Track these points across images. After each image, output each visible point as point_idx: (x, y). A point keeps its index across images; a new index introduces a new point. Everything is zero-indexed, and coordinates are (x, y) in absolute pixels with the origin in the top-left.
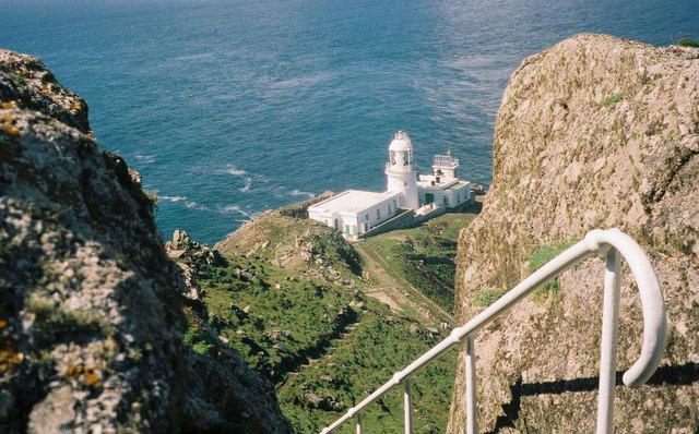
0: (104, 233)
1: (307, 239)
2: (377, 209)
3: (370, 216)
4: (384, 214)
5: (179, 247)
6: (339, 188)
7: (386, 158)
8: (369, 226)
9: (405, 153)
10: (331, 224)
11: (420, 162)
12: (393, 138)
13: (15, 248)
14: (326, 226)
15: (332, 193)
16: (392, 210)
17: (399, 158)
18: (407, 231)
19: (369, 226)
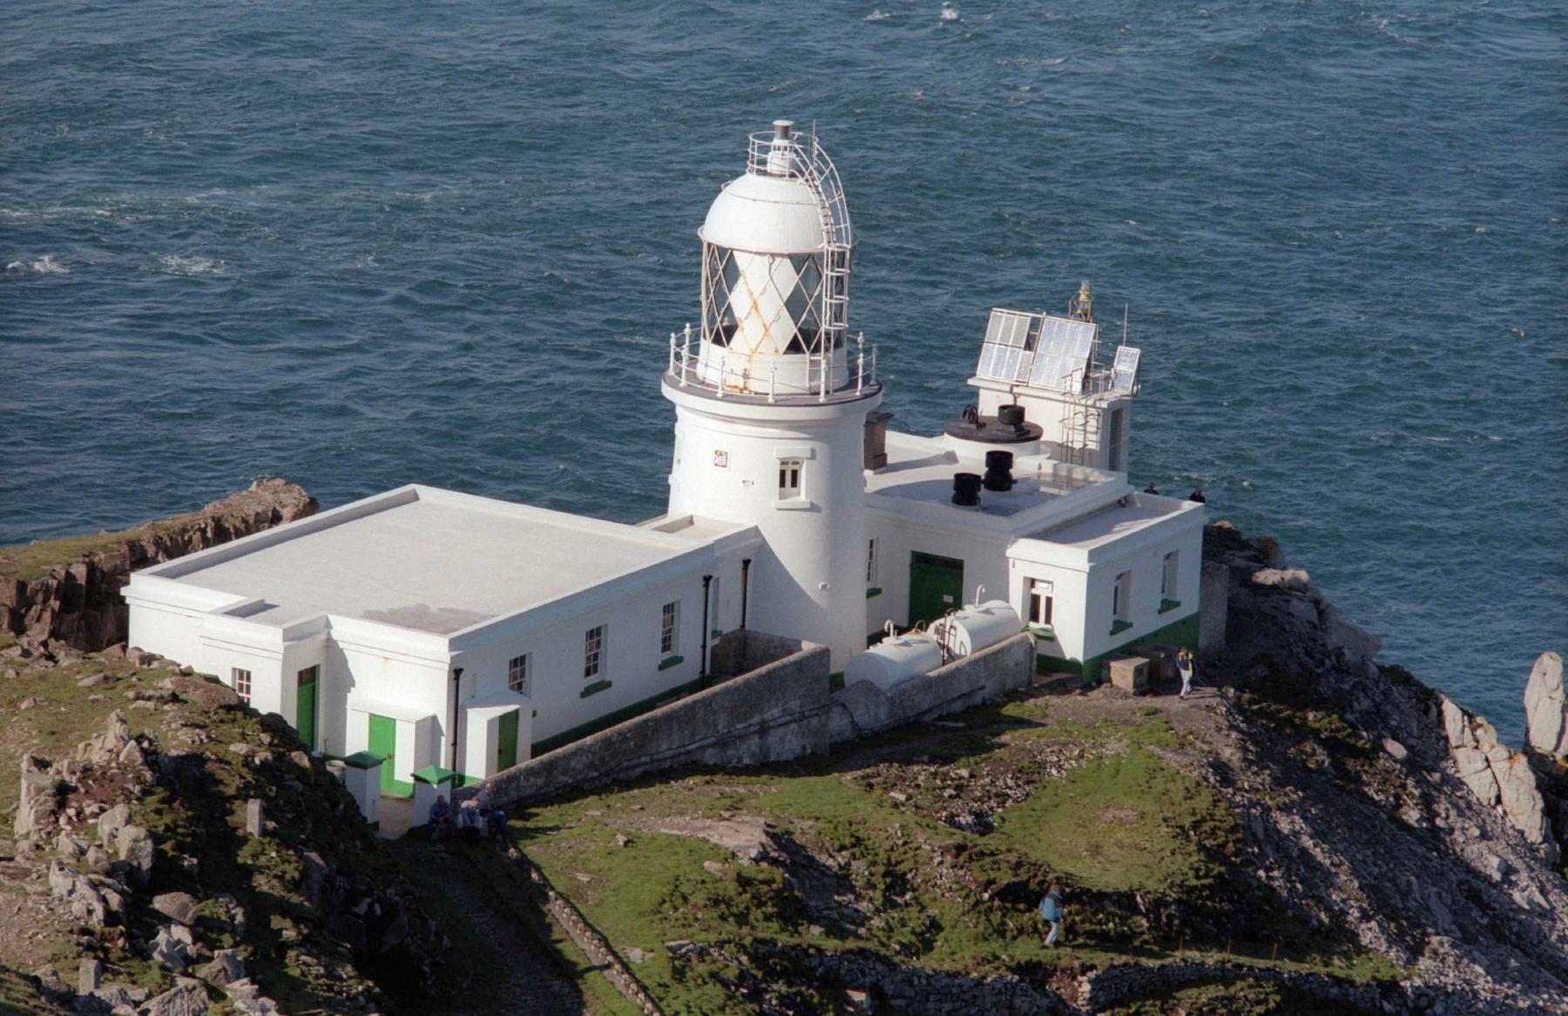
0: (1290, 978)
1: (97, 782)
2: (589, 623)
3: (536, 676)
4: (634, 669)
5: (1183, 960)
6: (340, 477)
7: (682, 290)
8: (525, 737)
9: (804, 263)
10: (227, 679)
11: (889, 349)
12: (733, 165)
13: (124, 904)
14: (243, 708)
15: (293, 497)
16: (689, 644)
17: (759, 298)
18: (782, 789)
19: (525, 737)
